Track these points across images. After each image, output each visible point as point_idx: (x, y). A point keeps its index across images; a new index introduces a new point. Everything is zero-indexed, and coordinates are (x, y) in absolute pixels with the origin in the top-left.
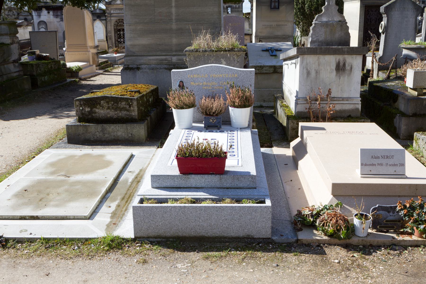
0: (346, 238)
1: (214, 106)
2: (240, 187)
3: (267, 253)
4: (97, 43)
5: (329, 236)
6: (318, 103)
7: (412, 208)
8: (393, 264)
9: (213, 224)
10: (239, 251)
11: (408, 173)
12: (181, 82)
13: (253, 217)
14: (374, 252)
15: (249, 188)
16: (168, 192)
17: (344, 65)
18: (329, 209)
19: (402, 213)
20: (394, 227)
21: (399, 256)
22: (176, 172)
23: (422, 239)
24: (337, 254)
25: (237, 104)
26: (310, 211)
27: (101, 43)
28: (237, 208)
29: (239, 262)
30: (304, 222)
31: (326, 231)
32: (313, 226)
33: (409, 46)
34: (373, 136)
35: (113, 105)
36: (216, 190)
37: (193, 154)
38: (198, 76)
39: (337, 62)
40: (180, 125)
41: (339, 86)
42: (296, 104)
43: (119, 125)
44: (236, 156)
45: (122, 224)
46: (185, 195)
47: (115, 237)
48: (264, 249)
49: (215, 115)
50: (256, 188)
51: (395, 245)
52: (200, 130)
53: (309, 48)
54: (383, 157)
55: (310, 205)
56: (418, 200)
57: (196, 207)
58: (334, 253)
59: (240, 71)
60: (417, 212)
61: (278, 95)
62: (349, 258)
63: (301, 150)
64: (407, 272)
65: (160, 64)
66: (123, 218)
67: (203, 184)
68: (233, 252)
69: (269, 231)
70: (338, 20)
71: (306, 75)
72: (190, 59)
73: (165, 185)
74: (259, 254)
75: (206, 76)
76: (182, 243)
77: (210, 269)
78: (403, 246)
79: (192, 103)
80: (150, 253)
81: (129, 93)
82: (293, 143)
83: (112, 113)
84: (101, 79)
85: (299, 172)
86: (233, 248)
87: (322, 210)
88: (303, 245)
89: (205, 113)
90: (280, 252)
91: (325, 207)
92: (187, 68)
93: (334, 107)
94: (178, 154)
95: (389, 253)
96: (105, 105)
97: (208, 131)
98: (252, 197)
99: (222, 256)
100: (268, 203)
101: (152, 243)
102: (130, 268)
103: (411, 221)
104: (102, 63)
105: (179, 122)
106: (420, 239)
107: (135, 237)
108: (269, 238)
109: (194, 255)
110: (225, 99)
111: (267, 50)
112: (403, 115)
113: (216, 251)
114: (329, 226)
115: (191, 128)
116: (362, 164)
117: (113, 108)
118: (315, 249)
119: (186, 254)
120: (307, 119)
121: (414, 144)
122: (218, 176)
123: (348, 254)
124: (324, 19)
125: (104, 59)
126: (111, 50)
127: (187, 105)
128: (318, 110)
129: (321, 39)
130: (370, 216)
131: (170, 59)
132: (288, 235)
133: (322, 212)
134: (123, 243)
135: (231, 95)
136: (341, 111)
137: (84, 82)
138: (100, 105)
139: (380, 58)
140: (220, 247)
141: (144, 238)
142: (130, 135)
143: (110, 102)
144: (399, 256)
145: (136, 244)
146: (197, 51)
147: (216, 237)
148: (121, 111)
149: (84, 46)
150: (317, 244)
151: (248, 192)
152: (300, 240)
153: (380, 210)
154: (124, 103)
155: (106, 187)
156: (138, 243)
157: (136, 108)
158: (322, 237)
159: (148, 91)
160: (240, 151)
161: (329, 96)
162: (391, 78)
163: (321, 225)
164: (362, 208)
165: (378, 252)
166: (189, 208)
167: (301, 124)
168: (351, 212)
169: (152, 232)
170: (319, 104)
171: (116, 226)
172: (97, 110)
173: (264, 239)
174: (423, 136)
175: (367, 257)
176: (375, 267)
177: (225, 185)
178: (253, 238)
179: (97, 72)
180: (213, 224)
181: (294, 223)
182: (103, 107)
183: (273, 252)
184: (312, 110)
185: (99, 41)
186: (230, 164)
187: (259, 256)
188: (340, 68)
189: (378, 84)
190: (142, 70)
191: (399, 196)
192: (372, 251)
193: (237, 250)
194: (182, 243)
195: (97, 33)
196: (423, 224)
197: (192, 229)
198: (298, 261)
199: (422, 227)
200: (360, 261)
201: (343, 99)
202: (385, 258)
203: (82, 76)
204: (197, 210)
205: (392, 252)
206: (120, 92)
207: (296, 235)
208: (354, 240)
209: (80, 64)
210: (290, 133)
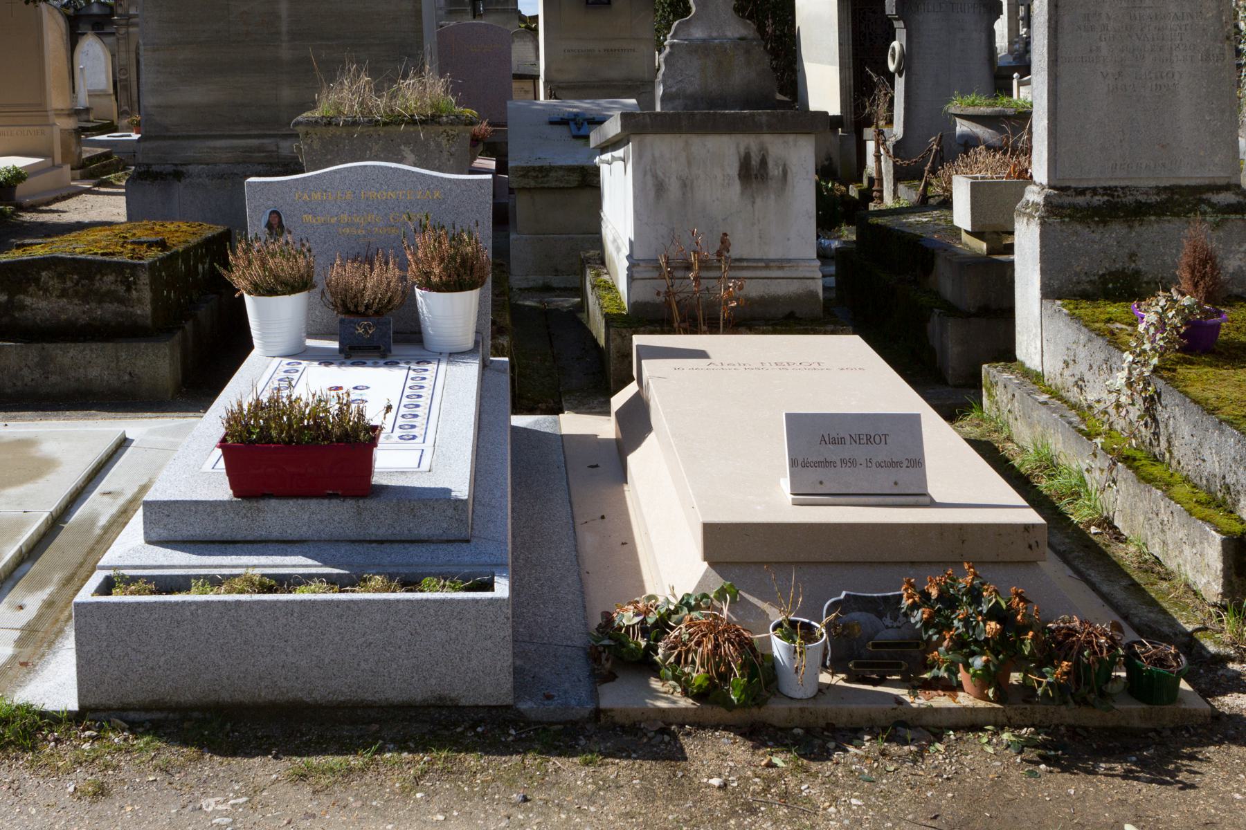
0: (747, 700)
1: (369, 285)
2: (419, 534)
3: (498, 758)
4: (83, 101)
5: (696, 697)
6: (691, 275)
7: (949, 601)
8: (896, 791)
9: (327, 661)
10: (410, 752)
11: (936, 489)
12: (275, 213)
13: (453, 636)
14: (838, 748)
15: (448, 541)
16: (194, 556)
17: (763, 162)
18: (697, 607)
19: (918, 616)
20: (899, 665)
21: (915, 762)
22: (223, 492)
23: (989, 705)
24: (720, 759)
25: (437, 279)
26: (637, 615)
27: (97, 100)
28: (401, 606)
29: (403, 788)
30: (622, 654)
31: (686, 681)
32: (645, 665)
33: (971, 111)
34: (850, 375)
35: (77, 284)
36: (344, 548)
37: (274, 433)
38: (326, 196)
39: (742, 153)
40: (265, 345)
41: (753, 224)
42: (631, 279)
43: (94, 346)
44: (419, 440)
45: (49, 663)
46: (247, 567)
47: (18, 707)
48: (490, 745)
49: (371, 312)
50: (468, 541)
51: (904, 724)
52: (326, 359)
53: (658, 114)
54: (856, 439)
55: (650, 591)
56: (965, 574)
57: (275, 603)
58: (711, 754)
59: (450, 180)
60: (961, 612)
61: (592, 253)
62: (759, 771)
63: (636, 422)
64: (936, 817)
65: (245, 162)
66: (58, 645)
67: (305, 529)
68: (388, 755)
69: (507, 683)
70: (737, 35)
71: (652, 194)
72: (310, 146)
73: (186, 532)
74: (472, 760)
75: (349, 196)
76: (228, 726)
77: (310, 816)
78: (927, 730)
79: (302, 277)
80: (123, 760)
81: (129, 247)
82: (618, 400)
83: (73, 310)
84: (76, 210)
85: (629, 491)
86: (393, 741)
87: (676, 612)
88: (614, 729)
89: (340, 309)
90: (541, 753)
91: (685, 603)
92: (303, 172)
93: (741, 288)
94: (227, 434)
95: (883, 754)
96: (54, 283)
97: (349, 361)
98: (454, 569)
99: (351, 770)
100: (502, 588)
101: (134, 728)
102: (47, 815)
103: (945, 643)
104: (91, 160)
105: (262, 337)
106: (981, 704)
107: (81, 707)
108: (508, 707)
109: (264, 765)
110: (403, 266)
111: (563, 122)
112: (951, 310)
113: (338, 753)
114: (693, 662)
115: (301, 353)
116: (793, 463)
117: (76, 293)
118: (653, 742)
119: (236, 763)
120: (665, 326)
121: (985, 399)
122: (349, 504)
123: (756, 758)
124: (698, 33)
125: (102, 146)
126: (125, 122)
127: (286, 284)
128: (692, 301)
129: (690, 90)
130: (820, 628)
131: (274, 148)
132: (574, 697)
133: (675, 618)
134: (40, 729)
135: (420, 254)
136: (763, 302)
137: (28, 217)
138: (37, 285)
139: (898, 145)
140: (351, 738)
141: (108, 709)
142: (127, 378)
143: (68, 276)
144: (915, 762)
145: (84, 731)
146: (330, 124)
147: (340, 706)
148: (100, 302)
149: (38, 110)
150: (661, 724)
151: (444, 554)
152: (605, 711)
153: (853, 610)
154: (110, 278)
155: (20, 543)
156: (89, 729)
157: (147, 295)
158: (674, 702)
159: (193, 240)
160: (427, 424)
161: (723, 255)
162: (932, 201)
163: (672, 659)
164: (795, 603)
165: (852, 750)
166: (251, 609)
167: (638, 340)
168: (764, 614)
169: (136, 691)
170: (695, 279)
171: (29, 673)
172: (28, 301)
173: (490, 708)
174: (1005, 375)
175: (814, 766)
176: (836, 799)
177: (375, 531)
178: (458, 707)
179: (75, 187)
180: (327, 661)
181: (593, 655)
182: (46, 290)
183: (518, 753)
184: (677, 298)
185: (92, 95)
186: (391, 463)
187: (469, 768)
188: (753, 173)
189: (881, 221)
190: (188, 180)
191: (912, 563)
192: (832, 745)
193: (401, 750)
194: (228, 726)
195: (86, 72)
196: (982, 654)
197: (261, 678)
198: (594, 783)
199: (978, 662)
200: (791, 781)
201: (768, 264)
202: (871, 770)
203: (26, 197)
204: (278, 613)
205: (894, 748)
206: (104, 243)
207: (594, 696)
208: (776, 711)
209: (21, 162)
210: (613, 365)
